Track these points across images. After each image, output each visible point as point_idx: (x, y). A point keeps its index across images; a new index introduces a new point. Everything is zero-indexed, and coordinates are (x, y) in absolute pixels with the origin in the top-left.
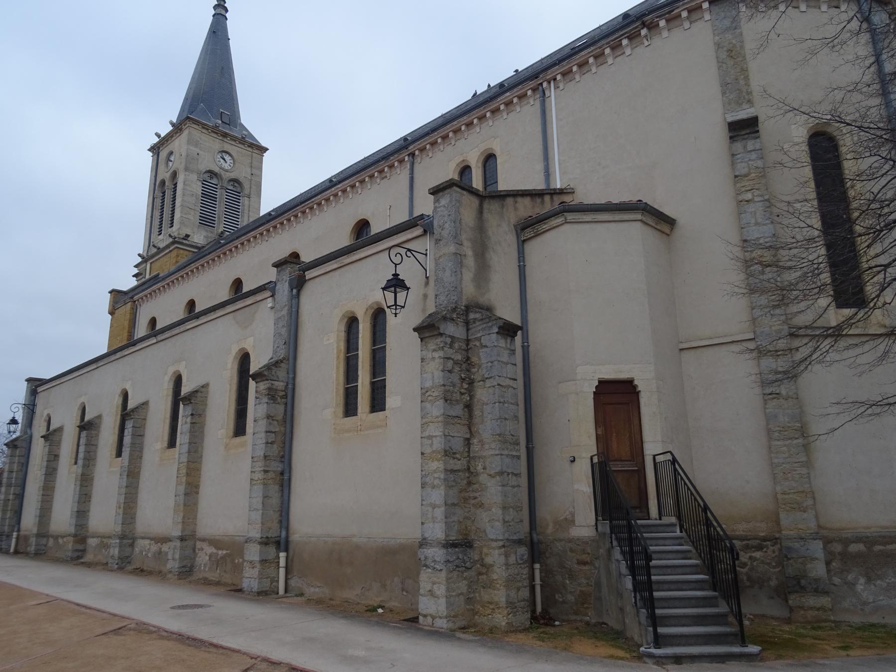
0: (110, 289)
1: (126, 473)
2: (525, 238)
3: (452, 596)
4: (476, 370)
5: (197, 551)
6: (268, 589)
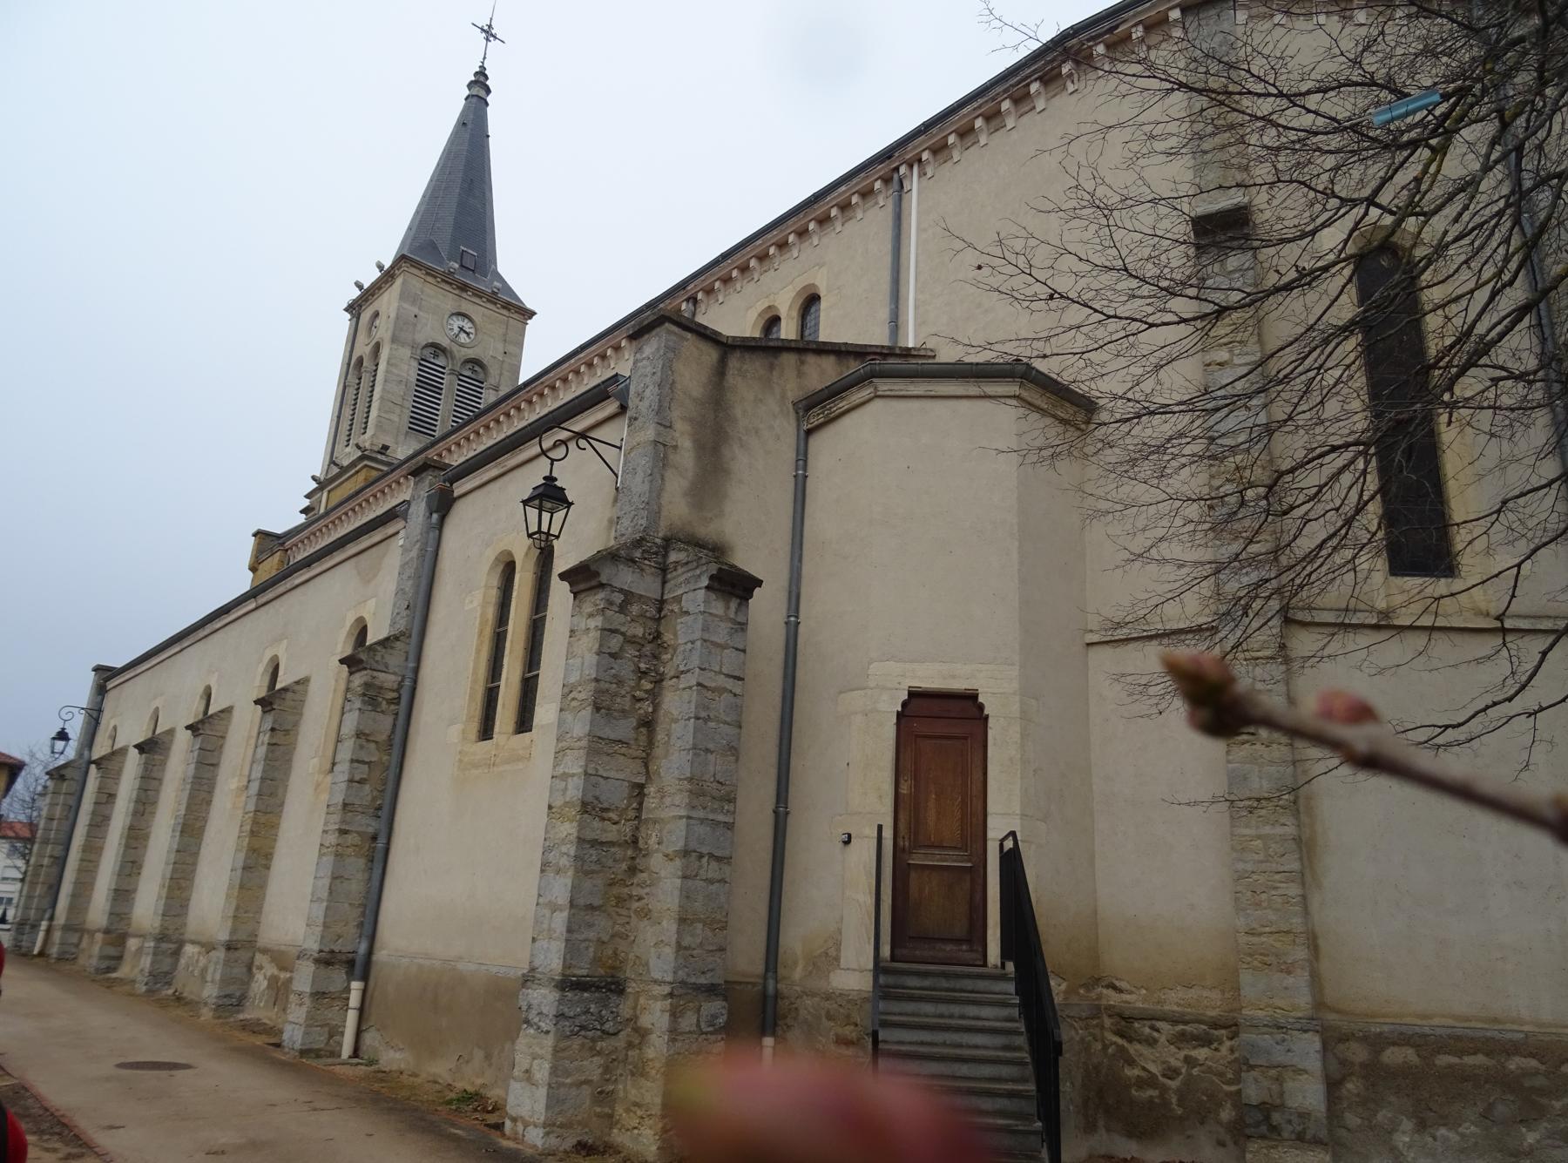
0: (254, 530)
1: (179, 829)
2: (809, 426)
3: (563, 1085)
4: (669, 656)
5: (254, 970)
6: (322, 1046)
